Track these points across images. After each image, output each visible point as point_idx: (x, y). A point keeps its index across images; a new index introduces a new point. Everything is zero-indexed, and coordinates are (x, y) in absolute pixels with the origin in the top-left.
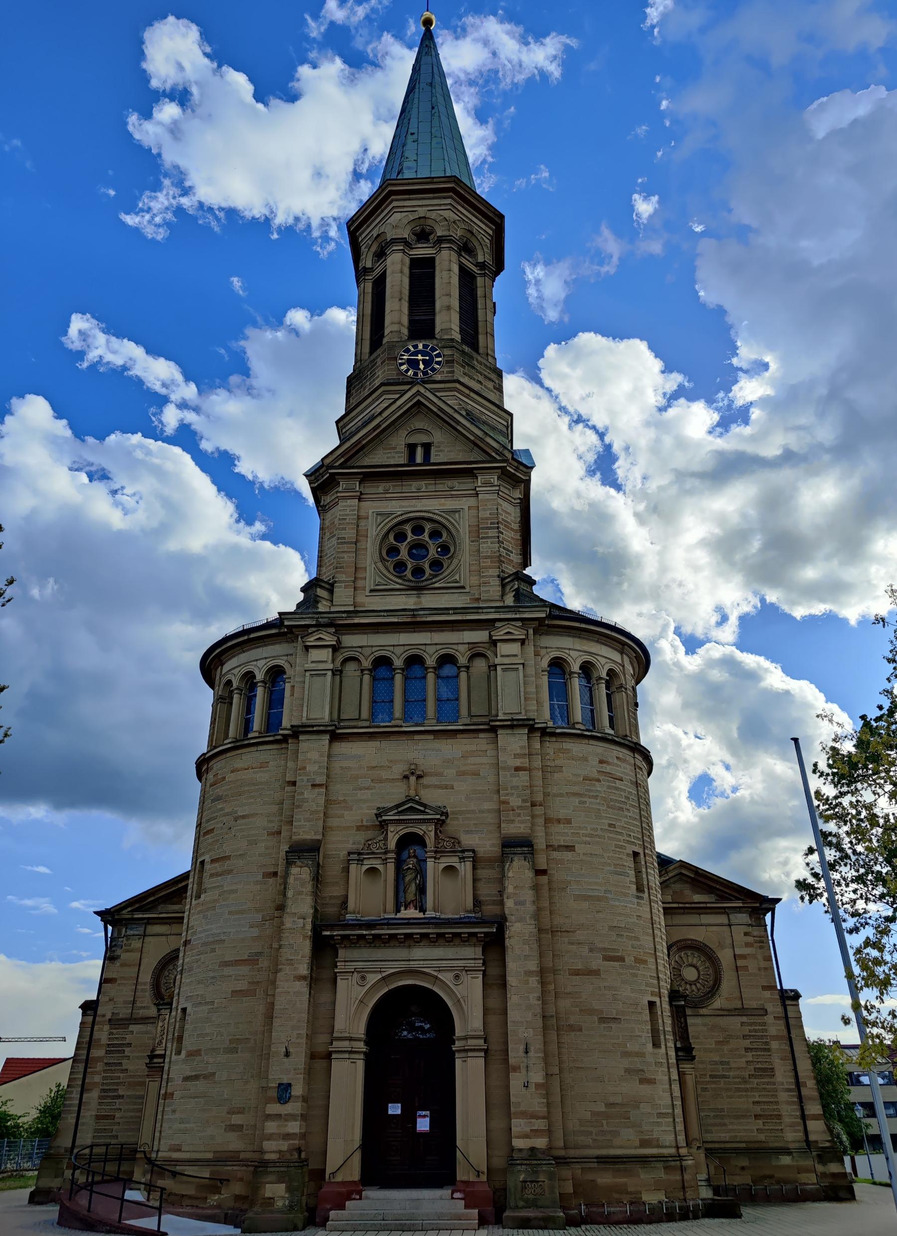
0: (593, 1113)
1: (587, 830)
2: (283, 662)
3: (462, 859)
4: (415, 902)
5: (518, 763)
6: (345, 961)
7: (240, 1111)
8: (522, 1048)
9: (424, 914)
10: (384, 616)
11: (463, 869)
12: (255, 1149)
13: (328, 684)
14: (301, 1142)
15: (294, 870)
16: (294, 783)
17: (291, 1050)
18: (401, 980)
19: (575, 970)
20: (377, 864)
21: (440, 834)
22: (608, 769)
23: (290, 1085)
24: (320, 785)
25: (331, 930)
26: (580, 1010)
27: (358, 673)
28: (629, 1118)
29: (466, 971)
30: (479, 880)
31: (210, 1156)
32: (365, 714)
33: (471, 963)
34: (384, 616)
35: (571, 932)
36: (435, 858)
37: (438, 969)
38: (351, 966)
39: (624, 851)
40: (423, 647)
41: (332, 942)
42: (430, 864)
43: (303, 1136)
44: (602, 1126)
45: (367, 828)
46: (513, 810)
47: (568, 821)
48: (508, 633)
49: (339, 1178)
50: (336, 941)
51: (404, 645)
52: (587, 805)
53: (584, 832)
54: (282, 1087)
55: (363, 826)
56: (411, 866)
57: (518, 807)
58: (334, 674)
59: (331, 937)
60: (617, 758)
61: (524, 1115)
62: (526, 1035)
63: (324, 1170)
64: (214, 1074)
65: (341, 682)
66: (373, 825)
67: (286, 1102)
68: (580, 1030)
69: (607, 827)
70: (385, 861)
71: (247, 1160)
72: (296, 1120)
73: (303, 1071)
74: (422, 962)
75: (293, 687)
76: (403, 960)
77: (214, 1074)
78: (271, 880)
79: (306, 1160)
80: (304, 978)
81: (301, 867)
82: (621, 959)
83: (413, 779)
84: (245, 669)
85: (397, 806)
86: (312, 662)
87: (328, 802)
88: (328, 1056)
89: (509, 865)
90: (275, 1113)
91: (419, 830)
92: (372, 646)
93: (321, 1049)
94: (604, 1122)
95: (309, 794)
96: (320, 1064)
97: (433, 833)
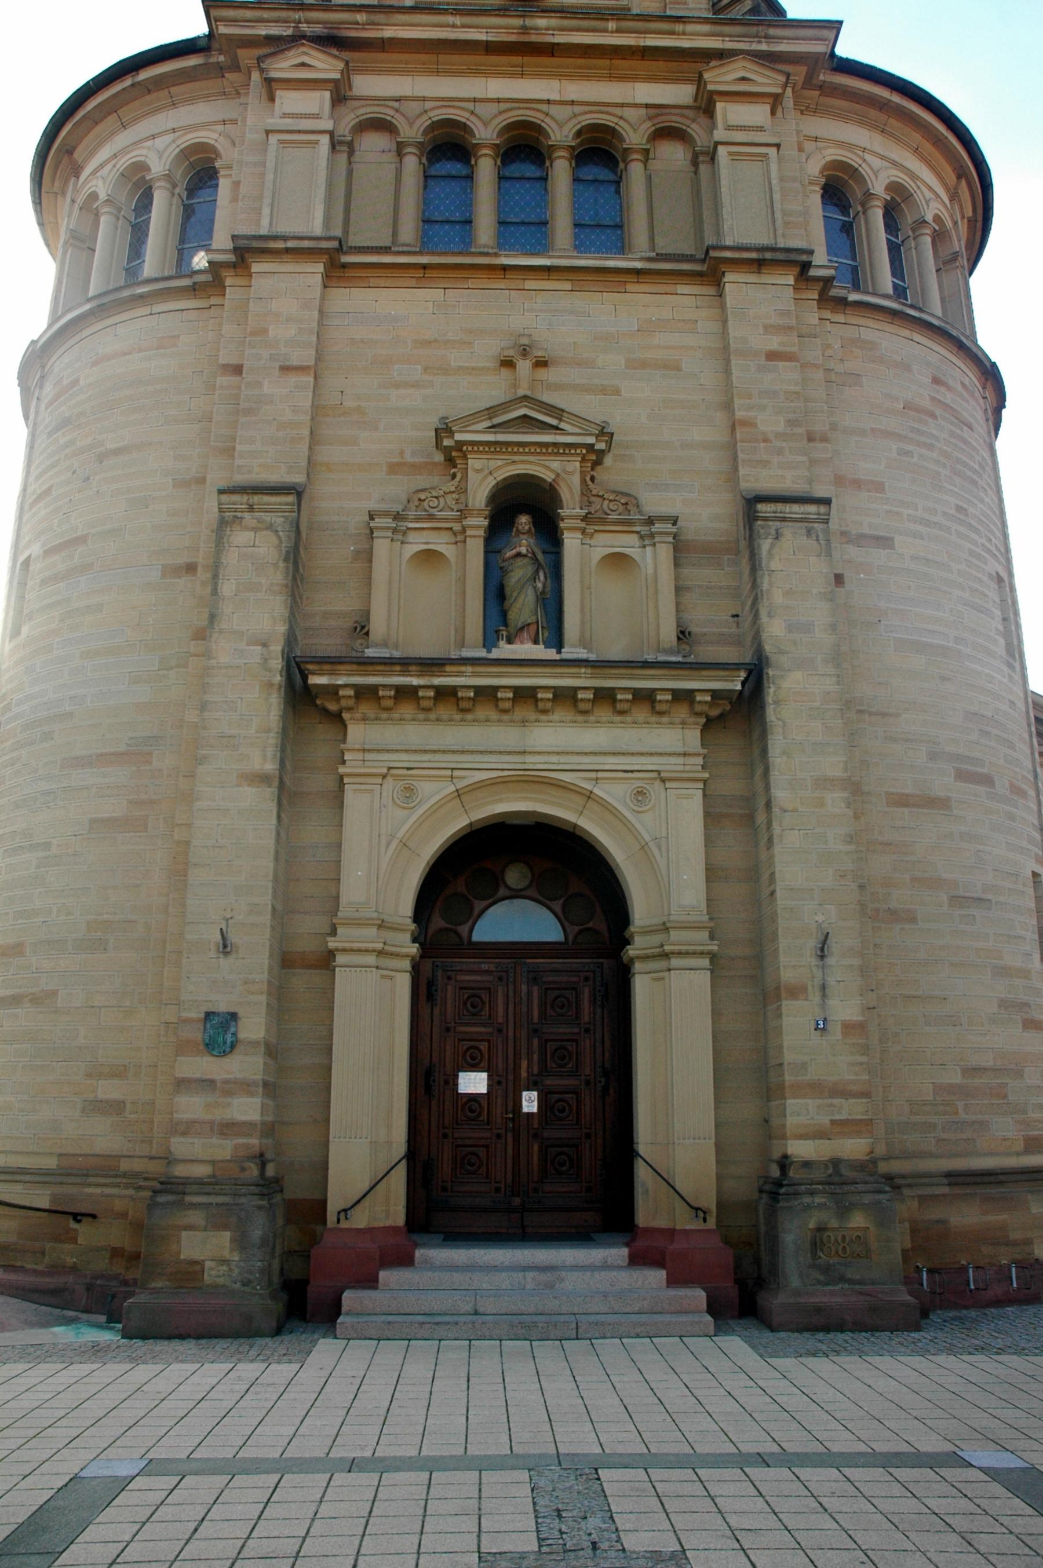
0: (938, 1089)
1: (916, 509)
2: (215, 136)
3: (648, 539)
4: (533, 628)
5: (774, 343)
6: (364, 750)
7: (119, 1073)
8: (812, 943)
9: (559, 652)
10: (454, 26)
11: (649, 560)
12: (154, 1153)
13: (323, 163)
14: (264, 1141)
15: (240, 537)
16: (238, 370)
17: (233, 937)
18: (501, 801)
19: (903, 794)
20: (441, 544)
21: (591, 485)
22: (948, 398)
23: (234, 1016)
24: (301, 369)
25: (332, 673)
26: (913, 880)
27: (392, 157)
28: (1005, 1097)
29: (663, 781)
30: (688, 589)
31: (51, 1163)
32: (409, 231)
33: (671, 765)
34: (454, 26)
35: (890, 715)
36: (583, 531)
37: (593, 775)
38: (379, 763)
39: (984, 566)
40: (544, 107)
41: (332, 707)
42: (571, 542)
43: (269, 1129)
44: (957, 1113)
45: (415, 468)
46: (765, 441)
47: (879, 487)
48: (743, 79)
49: (360, 1220)
50: (344, 703)
51: (499, 101)
52: (915, 459)
53: (911, 512)
54: (216, 1020)
55: (404, 464)
56: (523, 550)
57: (778, 435)
58: (333, 146)
59: (333, 691)
60: (962, 383)
61: (817, 1089)
62: (820, 918)
63: (323, 1203)
64: (55, 993)
65: (350, 173)
66: (426, 463)
67: (224, 1054)
68: (913, 920)
69: (953, 512)
70: (460, 537)
71: (136, 1175)
72: (252, 1095)
73: (265, 987)
74: (554, 759)
75: (237, 184)
76: (510, 753)
77: (55, 993)
78: (183, 582)
79: (277, 1180)
80: (263, 779)
81: (255, 530)
82: (987, 780)
83: (524, 366)
84: (124, 162)
85: (491, 411)
86: (285, 115)
87: (317, 411)
88: (326, 961)
89: (772, 546)
90: (198, 1075)
91: (544, 469)
92: (424, 99)
93: (307, 945)
94: (960, 1105)
95: (275, 387)
96: (302, 981)
97: (576, 480)
